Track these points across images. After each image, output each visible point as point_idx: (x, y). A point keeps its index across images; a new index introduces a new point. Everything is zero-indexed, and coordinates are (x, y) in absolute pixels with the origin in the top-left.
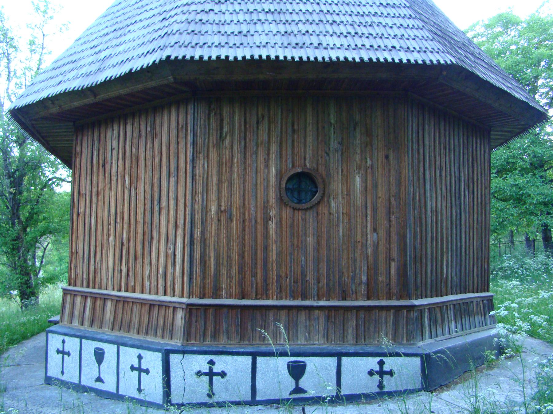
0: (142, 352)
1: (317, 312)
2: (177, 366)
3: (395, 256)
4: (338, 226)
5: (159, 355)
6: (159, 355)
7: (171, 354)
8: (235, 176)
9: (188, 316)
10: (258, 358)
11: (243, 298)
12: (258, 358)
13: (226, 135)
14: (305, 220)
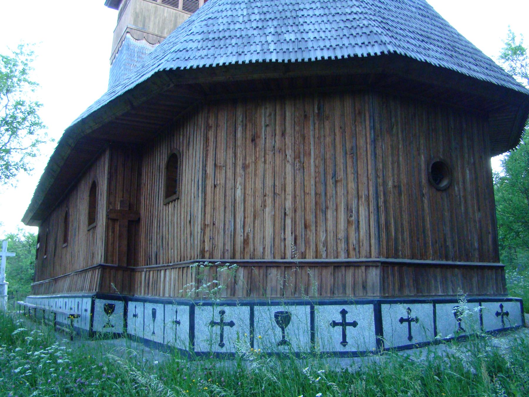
0: (345, 307)
1: (456, 270)
2: (386, 315)
3: (490, 231)
4: (460, 205)
5: (371, 306)
6: (371, 306)
7: (382, 305)
8: (401, 158)
9: (382, 273)
10: (437, 305)
11: (413, 259)
12: (437, 305)
13: (394, 125)
14: (101, 261)
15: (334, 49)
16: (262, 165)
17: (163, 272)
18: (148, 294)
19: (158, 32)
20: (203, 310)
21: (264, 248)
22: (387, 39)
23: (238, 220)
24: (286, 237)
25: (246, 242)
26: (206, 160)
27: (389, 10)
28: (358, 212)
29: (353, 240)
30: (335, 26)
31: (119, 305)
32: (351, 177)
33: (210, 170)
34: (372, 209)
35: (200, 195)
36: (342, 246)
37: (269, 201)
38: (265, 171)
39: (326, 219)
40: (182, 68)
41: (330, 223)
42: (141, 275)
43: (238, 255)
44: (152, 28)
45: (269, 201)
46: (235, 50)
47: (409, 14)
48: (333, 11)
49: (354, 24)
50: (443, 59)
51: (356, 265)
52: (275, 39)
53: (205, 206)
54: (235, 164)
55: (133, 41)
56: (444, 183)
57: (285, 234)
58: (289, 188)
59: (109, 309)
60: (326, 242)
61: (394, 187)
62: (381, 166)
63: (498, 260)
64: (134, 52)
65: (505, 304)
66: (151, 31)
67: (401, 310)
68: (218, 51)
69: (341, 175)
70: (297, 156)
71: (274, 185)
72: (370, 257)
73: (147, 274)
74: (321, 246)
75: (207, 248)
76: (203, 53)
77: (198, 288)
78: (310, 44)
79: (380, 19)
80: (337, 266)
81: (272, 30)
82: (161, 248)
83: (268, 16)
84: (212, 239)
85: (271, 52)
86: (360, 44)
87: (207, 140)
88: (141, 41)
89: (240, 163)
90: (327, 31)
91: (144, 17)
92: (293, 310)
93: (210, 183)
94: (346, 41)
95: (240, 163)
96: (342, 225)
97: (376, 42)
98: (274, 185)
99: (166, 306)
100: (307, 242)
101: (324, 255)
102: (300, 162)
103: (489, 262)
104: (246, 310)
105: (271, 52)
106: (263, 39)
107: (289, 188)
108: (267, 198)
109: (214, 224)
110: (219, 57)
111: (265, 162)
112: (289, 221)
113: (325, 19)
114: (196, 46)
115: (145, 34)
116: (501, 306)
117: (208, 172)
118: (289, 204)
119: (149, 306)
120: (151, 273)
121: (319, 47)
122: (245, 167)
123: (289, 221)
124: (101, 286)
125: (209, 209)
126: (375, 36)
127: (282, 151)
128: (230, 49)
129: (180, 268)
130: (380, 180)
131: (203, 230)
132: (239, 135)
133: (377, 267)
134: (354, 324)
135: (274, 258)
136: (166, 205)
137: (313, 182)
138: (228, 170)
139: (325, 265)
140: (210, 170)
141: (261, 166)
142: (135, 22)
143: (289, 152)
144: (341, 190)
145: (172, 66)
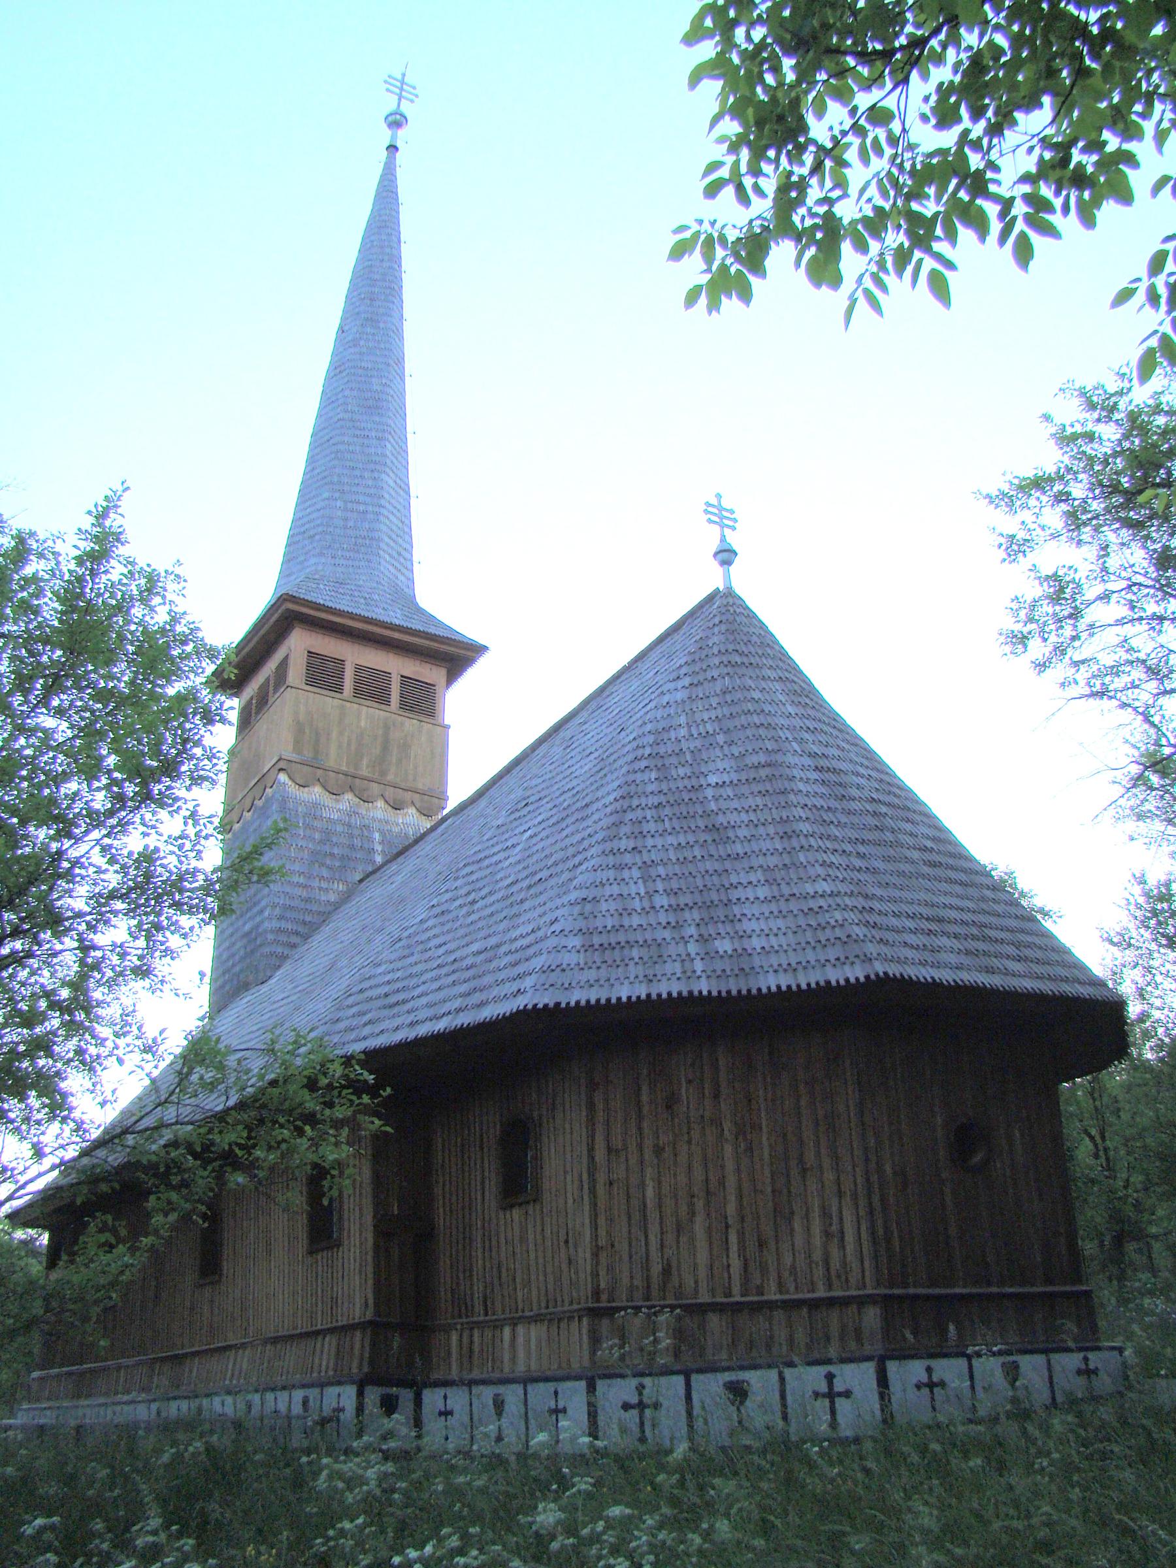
15: (795, 970)
16: (685, 1147)
17: (507, 1331)
18: (471, 1370)
19: (348, 765)
20: (609, 1386)
21: (696, 1282)
22: (872, 949)
23: (652, 1237)
24: (731, 1262)
25: (667, 1271)
26: (593, 1137)
27: (875, 871)
28: (841, 1219)
29: (835, 1264)
30: (790, 921)
31: (406, 1396)
32: (827, 1162)
33: (600, 1154)
34: (862, 1213)
35: (586, 1197)
36: (819, 1272)
37: (700, 1204)
38: (690, 1155)
39: (792, 1230)
40: (563, 1005)
41: (799, 1240)
42: (449, 1339)
43: (655, 1292)
44: (334, 757)
45: (700, 1204)
46: (640, 971)
47: (907, 868)
48: (786, 891)
49: (821, 919)
50: (959, 967)
51: (845, 1302)
52: (646, 827)
53: (596, 1215)
54: (640, 1147)
55: (292, 789)
56: (977, 1158)
57: (728, 1256)
58: (731, 1181)
59: (389, 1406)
60: (793, 1267)
61: (895, 1173)
62: (872, 1142)
63: (1078, 1280)
64: (297, 815)
65: (1090, 1355)
66: (331, 763)
67: (916, 1369)
68: (614, 974)
69: (810, 1157)
70: (740, 1132)
71: (707, 1180)
72: (865, 1287)
73: (466, 1334)
74: (786, 1274)
75: (603, 1285)
76: (592, 975)
77: (622, 1347)
78: (757, 961)
79: (860, 902)
80: (814, 1305)
81: (692, 930)
82: (497, 1288)
83: (683, 900)
84: (610, 1269)
85: (699, 977)
86: (833, 961)
87: (591, 1106)
88: (311, 789)
89: (648, 1143)
90: (780, 933)
91: (317, 734)
92: (753, 1378)
93: (601, 1178)
94: (810, 956)
95: (648, 1143)
96: (817, 1240)
97: (857, 956)
98: (707, 1180)
99: (529, 1388)
100: (764, 1270)
101: (792, 1289)
102: (745, 1139)
103: (1065, 1284)
104: (679, 1380)
105: (699, 977)
106: (681, 949)
107: (731, 1181)
108: (695, 1200)
109: (613, 1246)
110: (617, 984)
111: (689, 1142)
112: (733, 1238)
113: (774, 907)
114: (575, 961)
115: (319, 772)
116: (1086, 1359)
117: (597, 1159)
118: (731, 1209)
119: (487, 1394)
120: (476, 1333)
121: (771, 966)
122: (658, 1151)
123: (733, 1238)
124: (372, 1362)
125: (602, 1221)
126: (855, 946)
127: (716, 1122)
128: (633, 970)
129: (550, 1321)
130: (873, 1165)
131: (596, 1255)
132: (645, 1098)
133: (875, 1303)
134: (847, 1394)
135: (714, 1296)
136: (504, 1209)
137: (767, 1173)
138: (630, 1156)
139: (797, 1304)
140: (600, 1154)
141: (683, 1149)
142: (298, 745)
143: (727, 1125)
144: (813, 1185)
145: (546, 1001)
